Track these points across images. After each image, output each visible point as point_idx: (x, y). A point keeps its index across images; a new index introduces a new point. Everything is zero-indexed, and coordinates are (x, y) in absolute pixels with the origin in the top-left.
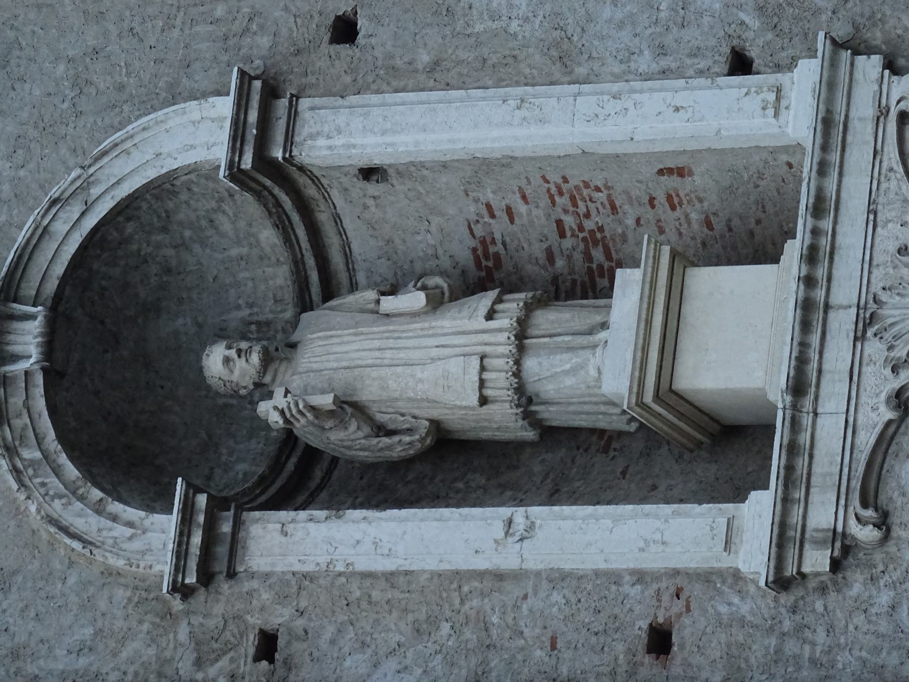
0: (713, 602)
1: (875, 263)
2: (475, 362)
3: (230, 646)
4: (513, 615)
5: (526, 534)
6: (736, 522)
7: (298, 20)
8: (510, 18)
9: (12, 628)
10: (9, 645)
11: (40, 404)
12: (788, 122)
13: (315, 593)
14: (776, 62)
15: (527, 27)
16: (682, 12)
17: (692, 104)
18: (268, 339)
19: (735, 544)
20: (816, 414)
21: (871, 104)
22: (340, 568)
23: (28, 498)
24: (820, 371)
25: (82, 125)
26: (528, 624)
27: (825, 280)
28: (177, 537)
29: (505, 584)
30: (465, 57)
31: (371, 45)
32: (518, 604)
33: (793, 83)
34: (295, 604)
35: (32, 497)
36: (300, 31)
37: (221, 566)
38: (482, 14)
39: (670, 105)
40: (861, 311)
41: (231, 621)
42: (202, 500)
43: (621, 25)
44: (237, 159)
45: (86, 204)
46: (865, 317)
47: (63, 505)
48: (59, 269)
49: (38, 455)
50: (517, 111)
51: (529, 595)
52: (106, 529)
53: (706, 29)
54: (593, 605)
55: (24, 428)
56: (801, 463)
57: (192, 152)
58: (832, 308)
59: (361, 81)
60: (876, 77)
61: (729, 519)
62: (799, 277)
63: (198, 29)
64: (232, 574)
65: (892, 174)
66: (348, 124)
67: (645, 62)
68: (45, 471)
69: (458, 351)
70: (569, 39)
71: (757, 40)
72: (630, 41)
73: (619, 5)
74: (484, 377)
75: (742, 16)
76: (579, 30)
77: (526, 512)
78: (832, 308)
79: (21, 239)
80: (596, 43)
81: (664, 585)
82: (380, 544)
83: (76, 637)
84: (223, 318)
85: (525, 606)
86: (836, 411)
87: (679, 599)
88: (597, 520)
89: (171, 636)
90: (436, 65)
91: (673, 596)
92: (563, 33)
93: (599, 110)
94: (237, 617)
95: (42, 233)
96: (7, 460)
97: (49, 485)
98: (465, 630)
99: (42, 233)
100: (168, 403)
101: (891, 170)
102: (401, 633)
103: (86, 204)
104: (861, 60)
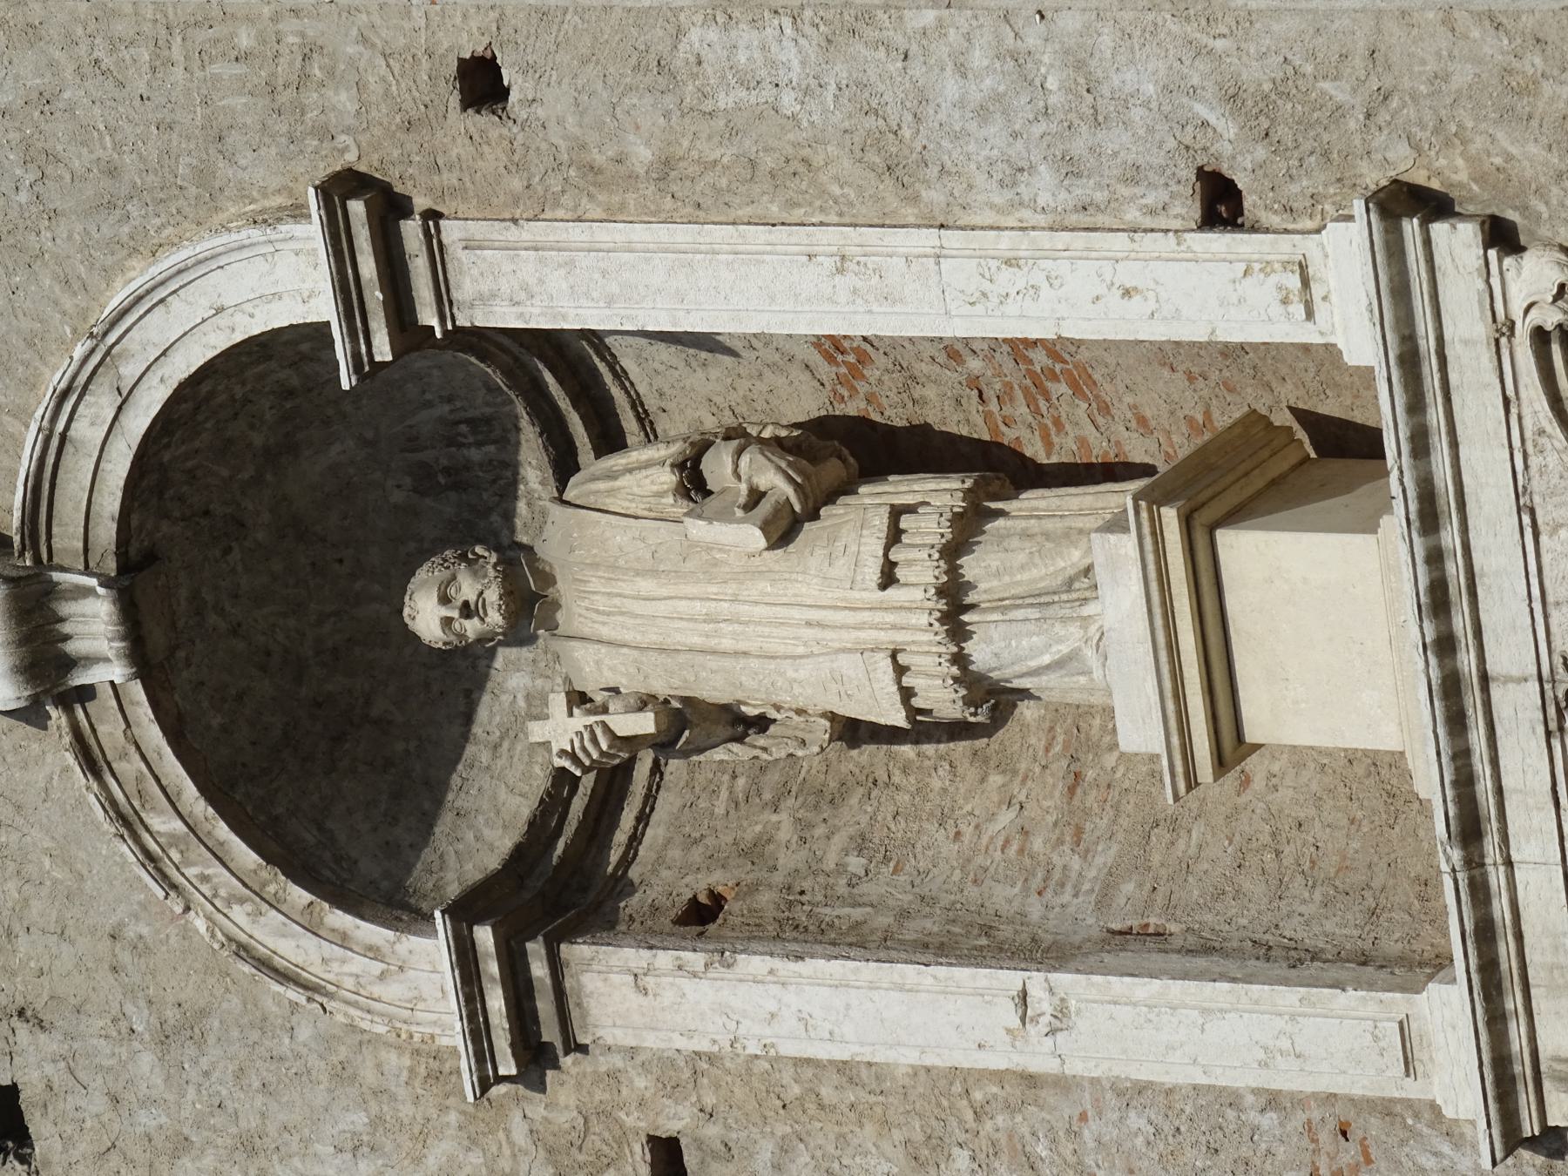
0: (1407, 1149)
1: (1550, 599)
2: (885, 665)
3: (605, 1161)
4: (1071, 1147)
5: (1057, 1024)
6: (1414, 1026)
7: (391, 62)
8: (777, 85)
9: (228, 1103)
10: (234, 1130)
11: (153, 735)
12: (1333, 325)
13: (724, 1084)
14: (1284, 201)
15: (812, 105)
16: (1089, 98)
17: (1152, 285)
18: (495, 442)
19: (1421, 1061)
20: (1509, 863)
21: (1477, 314)
22: (754, 1048)
23: (187, 909)
24: (1499, 791)
25: (65, 236)
26: (1100, 1163)
27: (1470, 636)
28: (463, 1010)
29: (1043, 1093)
30: (716, 154)
31: (538, 119)
32: (1075, 1128)
33: (1326, 256)
34: (694, 1099)
35: (192, 906)
36: (403, 85)
37: (550, 1033)
38: (723, 77)
39: (1112, 284)
40: (1547, 687)
41: (593, 1120)
42: (484, 936)
43: (982, 113)
44: (363, 348)
45: (120, 394)
46: (1556, 697)
47: (249, 914)
48: (110, 502)
49: (178, 825)
50: (838, 278)
51: (1089, 1114)
52: (336, 960)
53: (1141, 132)
54: (1203, 1139)
55: (139, 779)
56: (1506, 949)
57: (276, 306)
58: (1496, 679)
59: (539, 188)
60: (1477, 266)
61: (1401, 1023)
62: (1424, 646)
63: (216, 68)
64: (574, 1046)
65: (1543, 440)
66: (541, 281)
67: (1044, 186)
68: (200, 855)
69: (849, 637)
70: (895, 133)
71: (1240, 158)
72: (1010, 145)
73: (970, 76)
74: (892, 557)
75: (1202, 111)
76: (910, 118)
77: (1046, 980)
78: (1496, 679)
79: (25, 465)
80: (945, 143)
81: (1316, 1115)
82: (811, 1022)
83: (341, 1127)
84: (408, 423)
85: (1086, 1133)
86: (1543, 860)
87: (1347, 1140)
88: (1174, 1008)
89: (501, 1135)
90: (665, 168)
91: (1336, 1135)
92: (881, 121)
93: (986, 286)
94: (604, 1114)
95: (56, 445)
96: (130, 842)
97: (215, 880)
98: (997, 1165)
99: (56, 445)
100: (358, 585)
101: (1542, 432)
102: (888, 1160)
103: (120, 394)
104: (1439, 229)
